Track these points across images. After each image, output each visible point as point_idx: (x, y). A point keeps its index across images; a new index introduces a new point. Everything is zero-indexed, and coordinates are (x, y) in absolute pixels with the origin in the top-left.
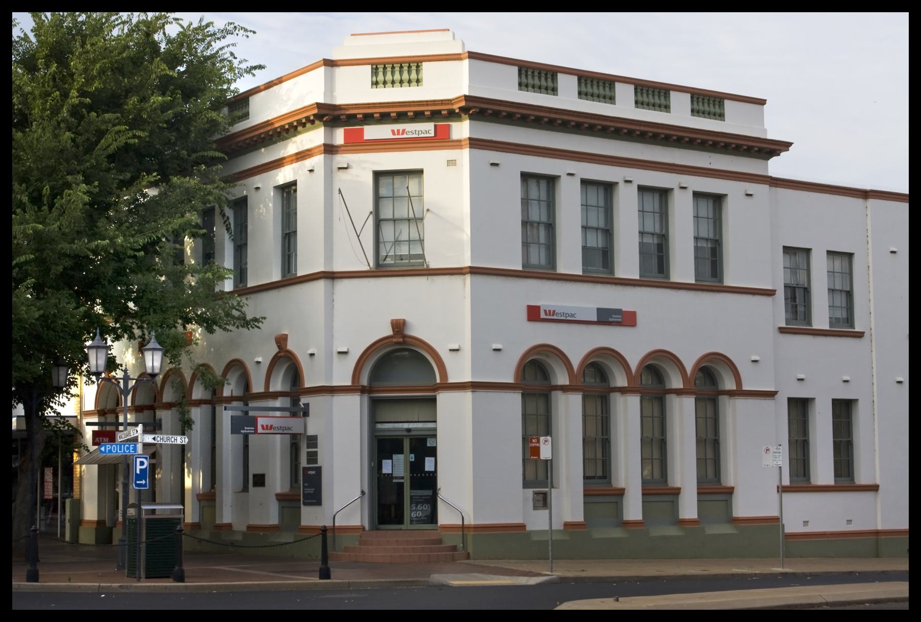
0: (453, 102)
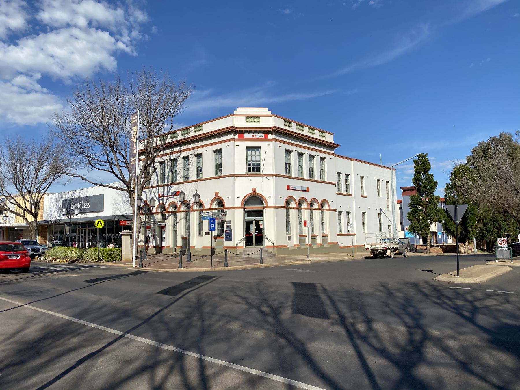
0: (235, 140)
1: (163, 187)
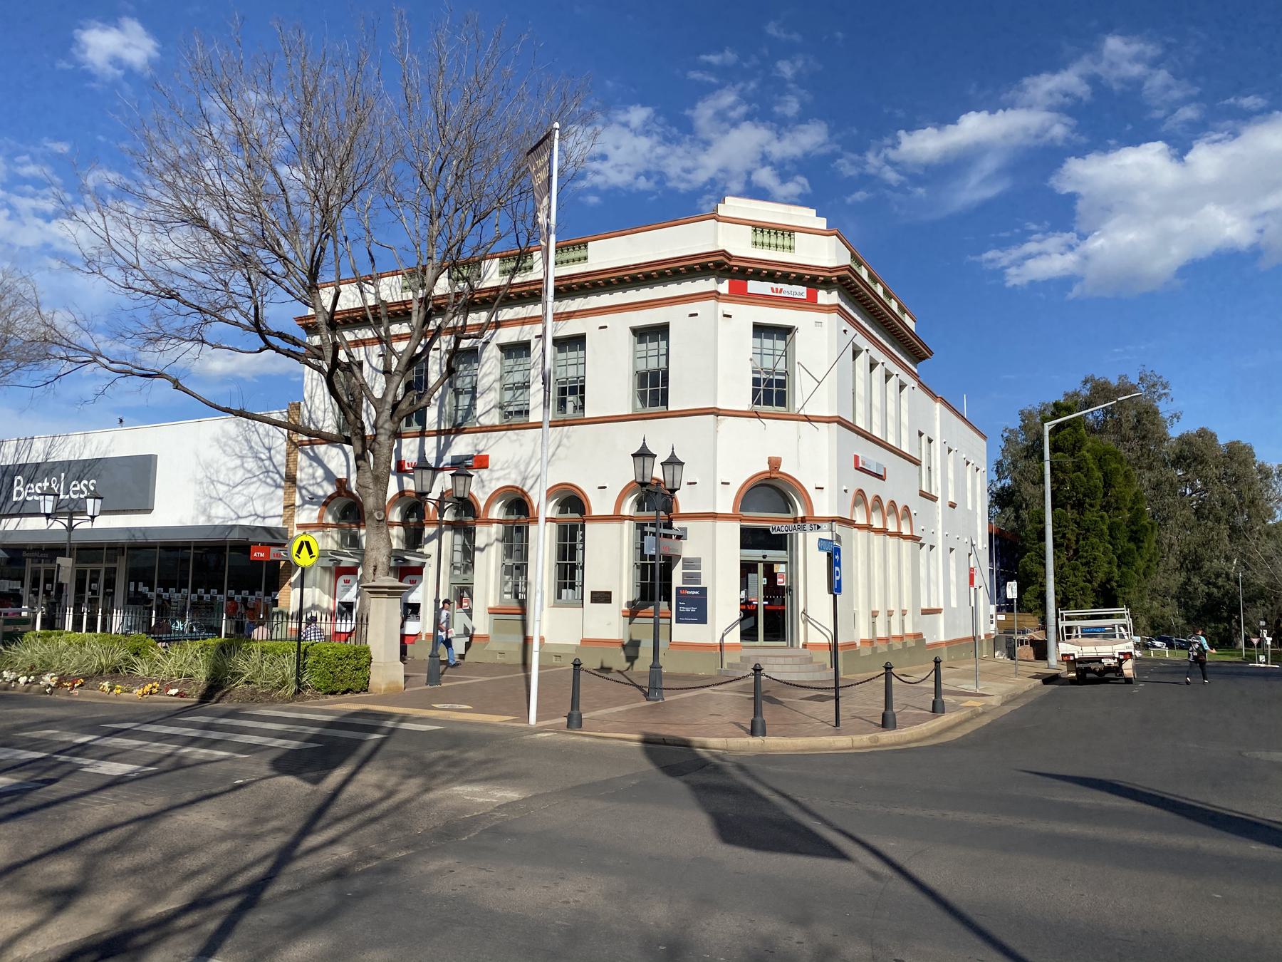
0: (720, 297)
1: (436, 438)
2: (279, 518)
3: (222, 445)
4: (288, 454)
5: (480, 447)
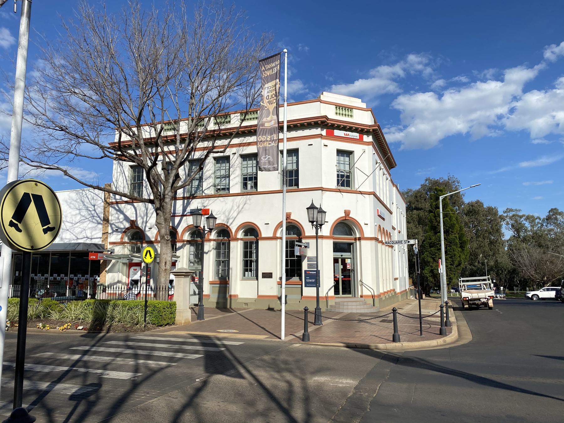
0: (322, 137)
1: (182, 201)
2: (99, 239)
3: (69, 203)
4: (105, 208)
5: (205, 205)
